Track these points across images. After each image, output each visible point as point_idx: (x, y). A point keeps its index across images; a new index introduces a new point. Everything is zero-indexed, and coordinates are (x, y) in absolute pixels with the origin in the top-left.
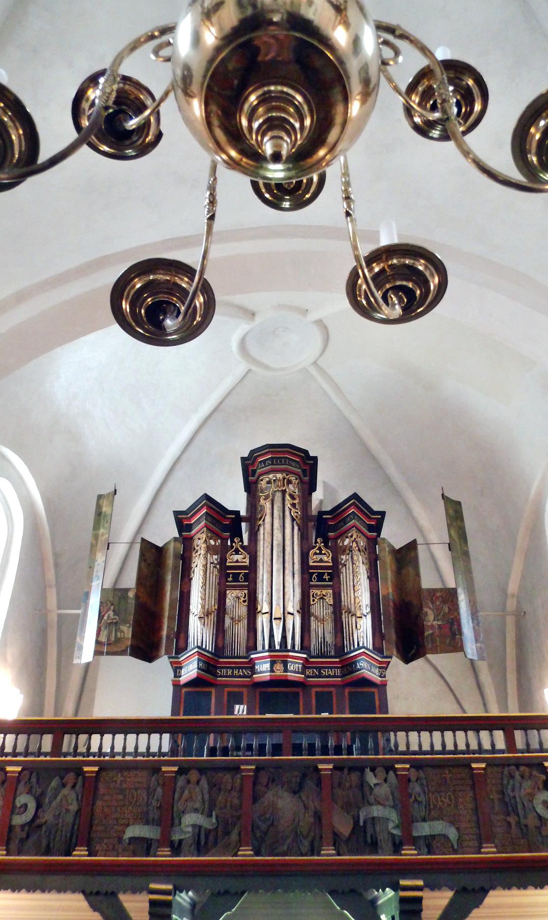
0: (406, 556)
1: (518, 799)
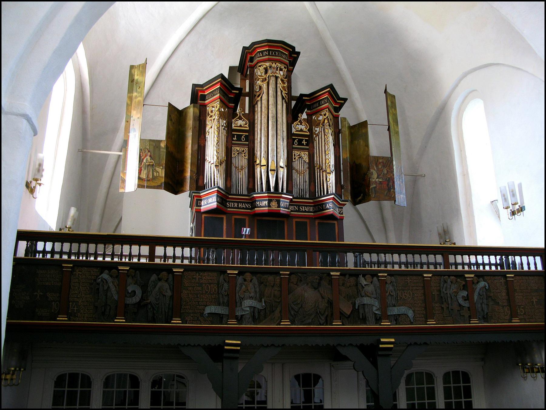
0: (359, 131)
1: (449, 295)
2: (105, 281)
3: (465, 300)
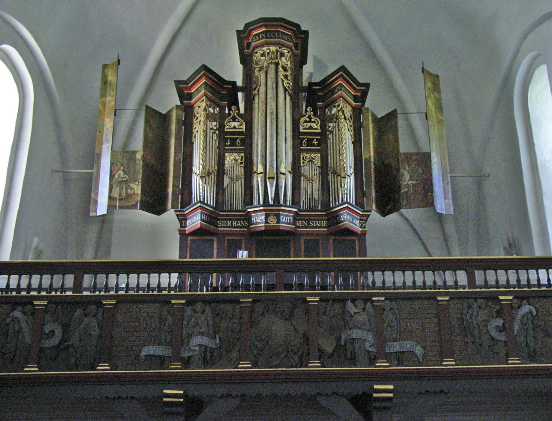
0: (386, 124)
1: (475, 325)
2: (15, 320)
3: (500, 331)
